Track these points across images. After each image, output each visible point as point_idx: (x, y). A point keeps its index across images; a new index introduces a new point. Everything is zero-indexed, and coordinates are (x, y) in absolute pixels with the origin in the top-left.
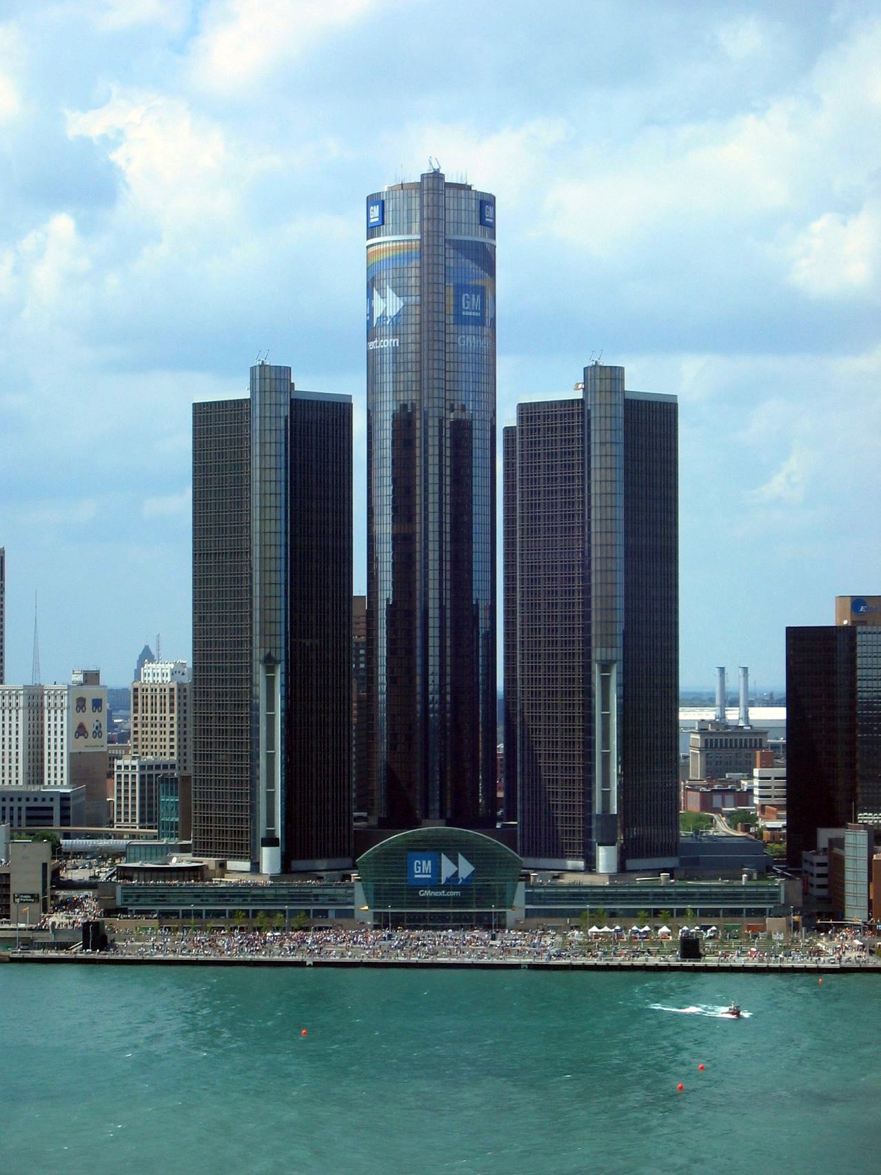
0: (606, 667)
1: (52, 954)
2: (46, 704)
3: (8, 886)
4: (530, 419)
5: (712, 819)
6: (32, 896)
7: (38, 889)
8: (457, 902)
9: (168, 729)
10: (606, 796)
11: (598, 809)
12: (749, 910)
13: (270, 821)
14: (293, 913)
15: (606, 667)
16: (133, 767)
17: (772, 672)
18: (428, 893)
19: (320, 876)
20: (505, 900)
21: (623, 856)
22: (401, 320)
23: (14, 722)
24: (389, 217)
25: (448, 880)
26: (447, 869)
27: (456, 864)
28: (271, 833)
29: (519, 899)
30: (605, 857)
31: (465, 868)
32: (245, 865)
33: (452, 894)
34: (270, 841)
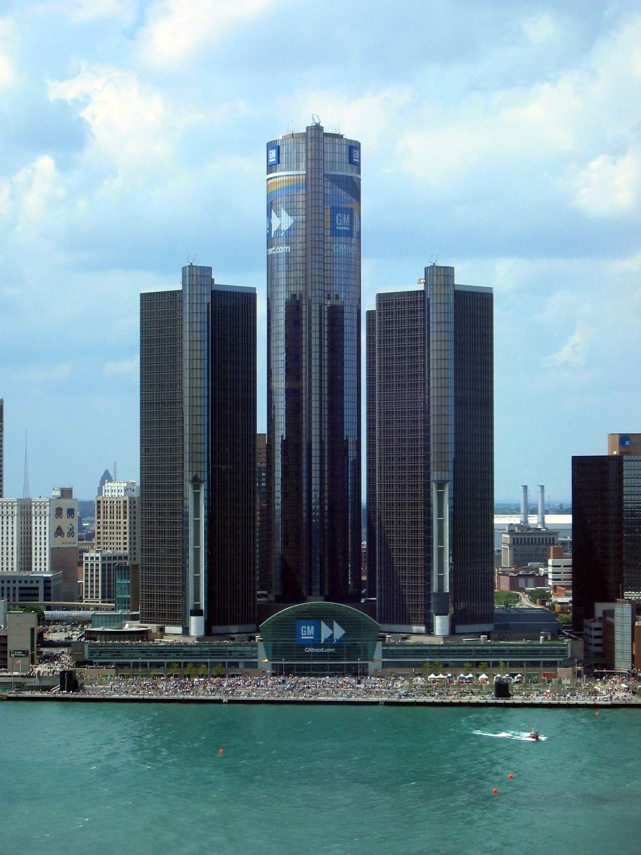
0: (441, 485)
1: (38, 694)
2: (33, 512)
3: (6, 645)
4: (385, 305)
5: (518, 596)
6: (24, 652)
7: (28, 647)
8: (333, 656)
9: (122, 530)
10: (441, 579)
11: (435, 589)
12: (545, 662)
13: (197, 598)
14: (213, 665)
15: (441, 485)
16: (97, 558)
17: (562, 489)
18: (311, 650)
19: (233, 637)
20: (367, 655)
21: (454, 623)
22: (292, 232)
23: (10, 525)
24: (283, 158)
25: (326, 640)
26: (325, 632)
27: (332, 628)
28: (197, 606)
29: (378, 655)
30: (440, 623)
31: (339, 632)
32: (179, 630)
33: (329, 650)
34: (197, 612)
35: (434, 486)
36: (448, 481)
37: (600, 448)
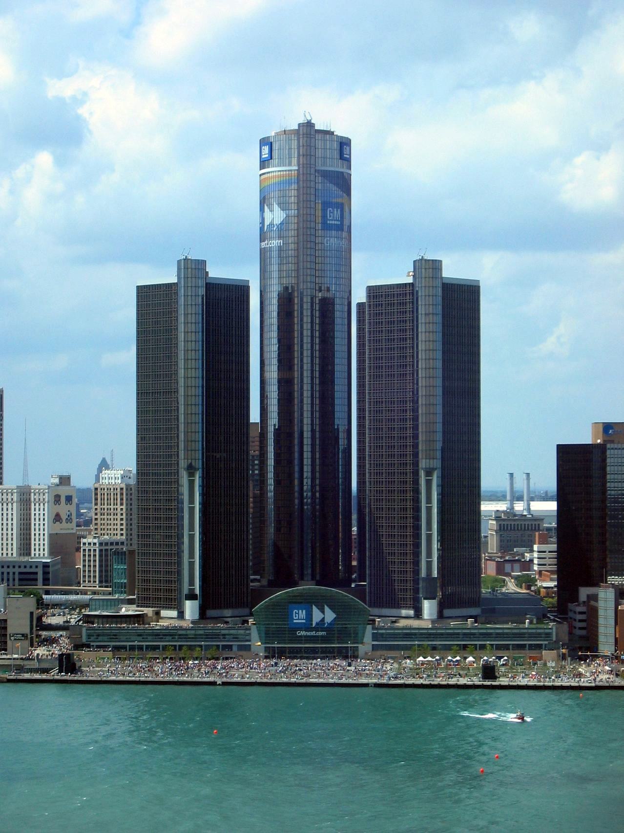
0: (429, 473)
1: (37, 676)
2: (32, 499)
3: (5, 628)
4: (375, 297)
5: (504, 581)
6: (23, 635)
7: (27, 631)
8: (324, 640)
9: (119, 517)
10: (429, 564)
12: (530, 645)
13: (192, 582)
14: (208, 647)
15: (429, 473)
16: (95, 544)
17: (547, 477)
18: (303, 633)
19: (227, 621)
20: (357, 638)
22: (284, 227)
23: (10, 512)
24: (275, 154)
25: (317, 624)
26: (317, 616)
27: (323, 612)
28: (192, 591)
29: (368, 638)
30: (429, 607)
31: (330, 616)
32: (174, 613)
33: (320, 633)
34: (192, 596)
35: (422, 474)
36: (436, 469)
37: (584, 436)
